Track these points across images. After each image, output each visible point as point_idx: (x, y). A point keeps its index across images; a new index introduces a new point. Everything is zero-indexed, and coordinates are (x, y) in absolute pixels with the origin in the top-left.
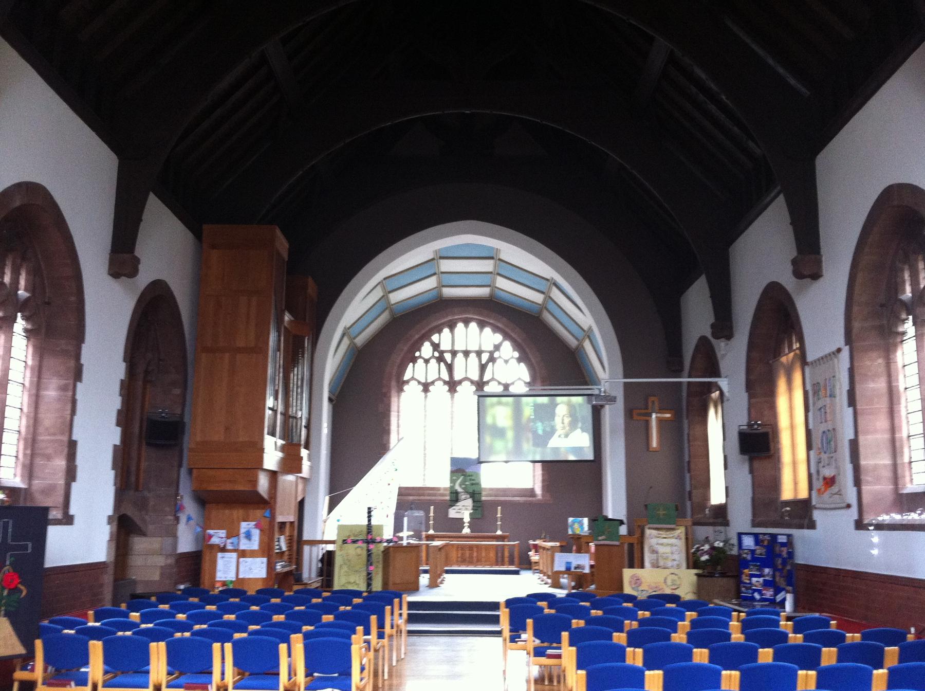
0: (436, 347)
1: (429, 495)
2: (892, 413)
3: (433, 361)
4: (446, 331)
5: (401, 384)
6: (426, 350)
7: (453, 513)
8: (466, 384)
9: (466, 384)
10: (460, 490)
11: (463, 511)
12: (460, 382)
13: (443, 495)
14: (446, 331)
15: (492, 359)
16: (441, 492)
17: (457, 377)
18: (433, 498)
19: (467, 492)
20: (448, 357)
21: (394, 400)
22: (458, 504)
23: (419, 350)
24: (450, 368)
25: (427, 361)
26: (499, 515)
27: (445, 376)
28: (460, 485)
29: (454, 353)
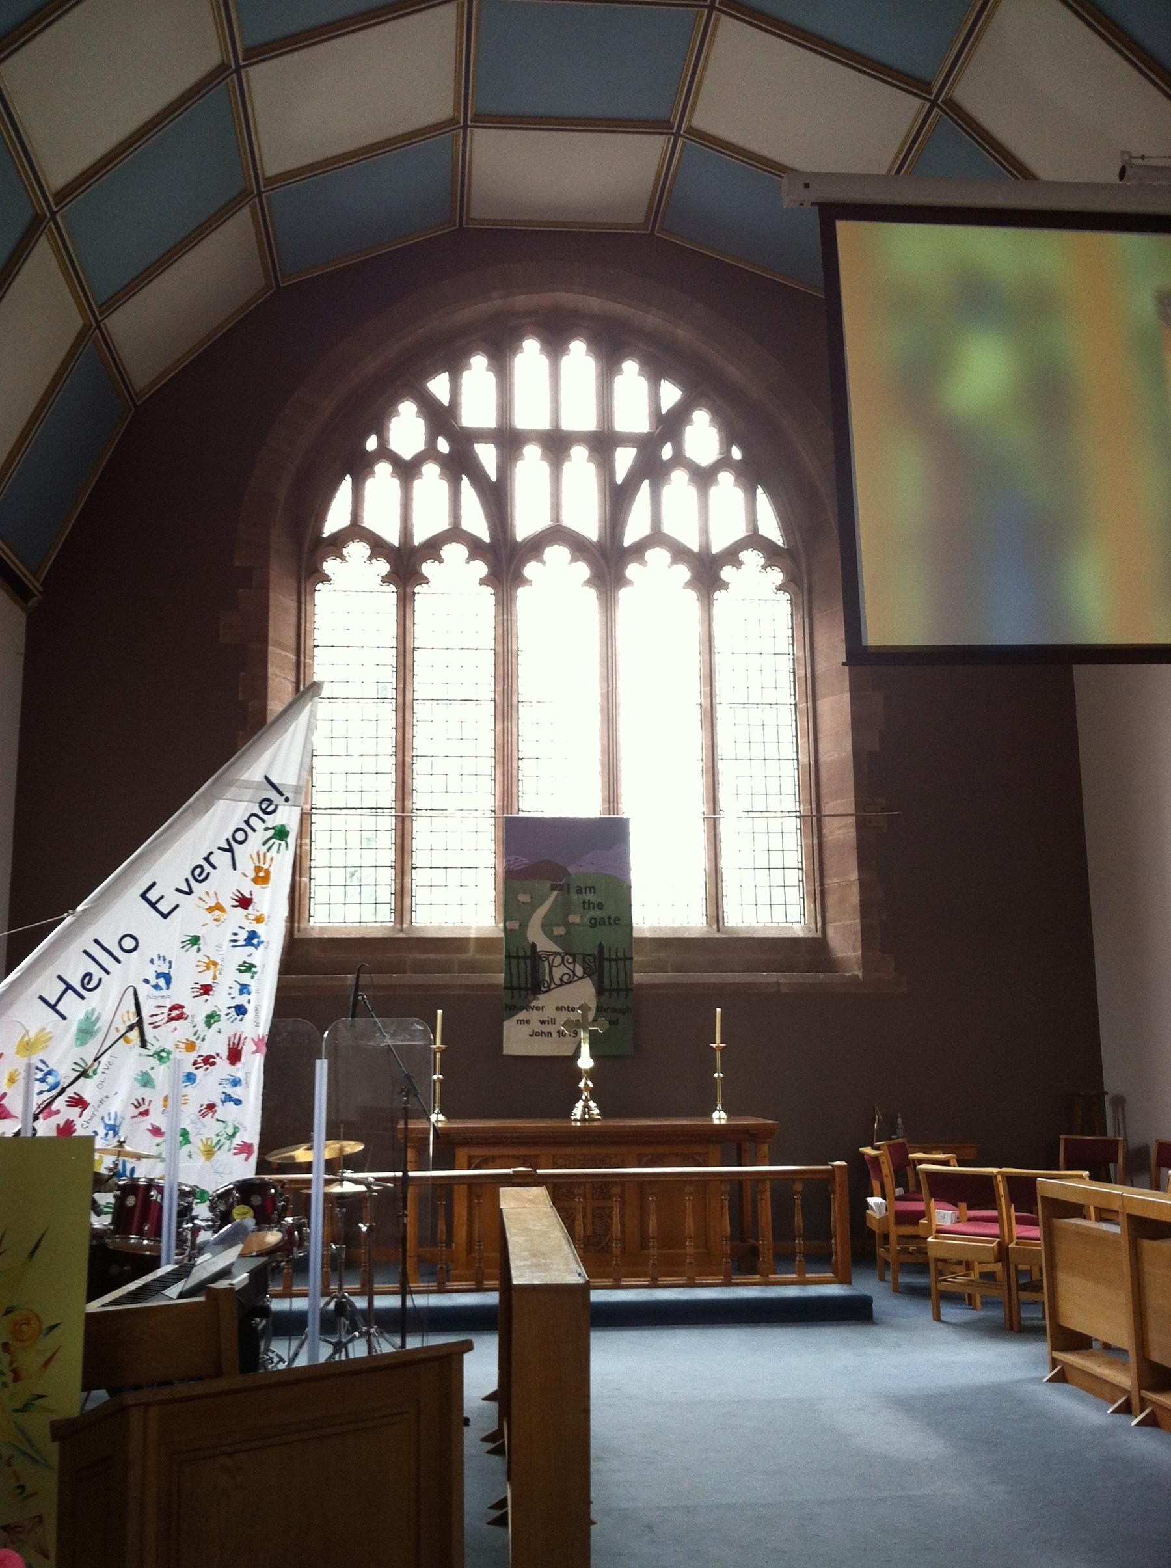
0: (441, 419)
1: (420, 967)
2: (398, 1414)
3: (431, 470)
4: (479, 362)
5: (309, 556)
6: (406, 429)
7: (518, 1039)
8: (557, 553)
9: (557, 553)
10: (544, 944)
11: (559, 1028)
12: (535, 547)
13: (471, 967)
14: (479, 362)
15: (651, 469)
16: (471, 954)
17: (524, 527)
18: (439, 978)
19: (570, 953)
20: (487, 455)
21: (281, 602)
22: (542, 1000)
23: (382, 432)
24: (497, 498)
25: (407, 471)
26: (718, 1043)
27: (476, 522)
28: (547, 927)
29: (509, 441)
